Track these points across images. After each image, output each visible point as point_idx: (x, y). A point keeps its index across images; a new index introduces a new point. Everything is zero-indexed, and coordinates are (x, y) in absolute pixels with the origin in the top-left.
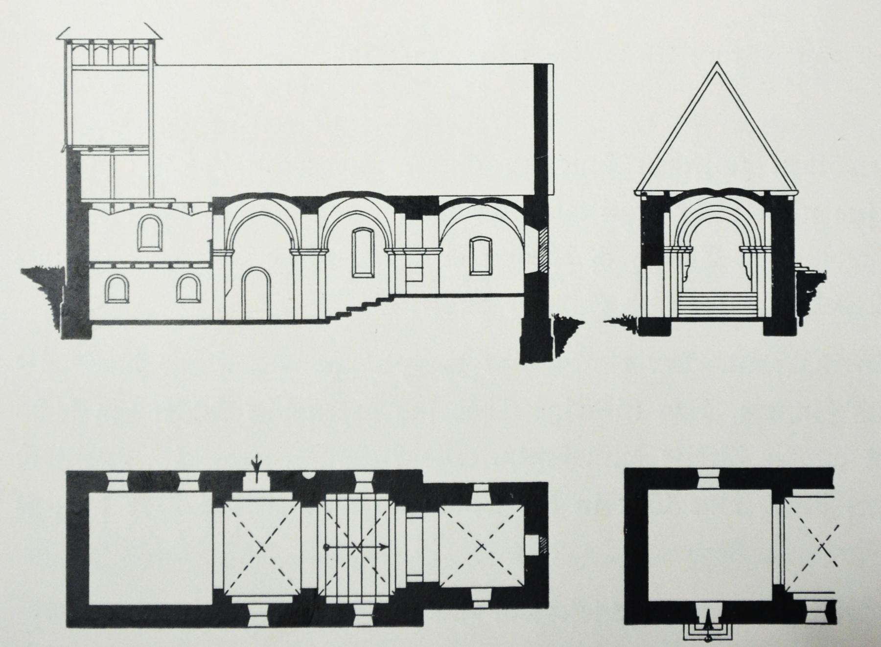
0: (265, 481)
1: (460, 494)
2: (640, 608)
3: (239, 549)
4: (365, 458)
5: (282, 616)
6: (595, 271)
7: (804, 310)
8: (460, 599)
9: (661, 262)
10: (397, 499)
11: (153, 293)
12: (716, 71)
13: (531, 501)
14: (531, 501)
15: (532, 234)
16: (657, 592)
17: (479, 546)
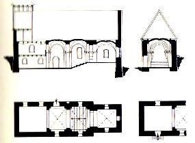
0: (58, 104)
1: (102, 107)
2: (143, 133)
3: (52, 119)
4: (81, 99)
5: (62, 134)
6: (132, 57)
7: (179, 66)
8: (102, 130)
9: (147, 55)
10: (88, 108)
11: (32, 62)
12: (159, 12)
13: (118, 108)
14: (118, 108)
15: (118, 49)
16: (146, 129)
17: (106, 118)
